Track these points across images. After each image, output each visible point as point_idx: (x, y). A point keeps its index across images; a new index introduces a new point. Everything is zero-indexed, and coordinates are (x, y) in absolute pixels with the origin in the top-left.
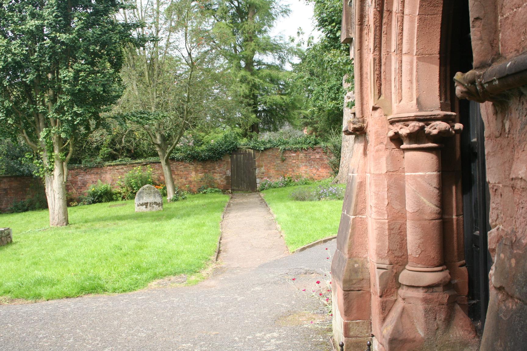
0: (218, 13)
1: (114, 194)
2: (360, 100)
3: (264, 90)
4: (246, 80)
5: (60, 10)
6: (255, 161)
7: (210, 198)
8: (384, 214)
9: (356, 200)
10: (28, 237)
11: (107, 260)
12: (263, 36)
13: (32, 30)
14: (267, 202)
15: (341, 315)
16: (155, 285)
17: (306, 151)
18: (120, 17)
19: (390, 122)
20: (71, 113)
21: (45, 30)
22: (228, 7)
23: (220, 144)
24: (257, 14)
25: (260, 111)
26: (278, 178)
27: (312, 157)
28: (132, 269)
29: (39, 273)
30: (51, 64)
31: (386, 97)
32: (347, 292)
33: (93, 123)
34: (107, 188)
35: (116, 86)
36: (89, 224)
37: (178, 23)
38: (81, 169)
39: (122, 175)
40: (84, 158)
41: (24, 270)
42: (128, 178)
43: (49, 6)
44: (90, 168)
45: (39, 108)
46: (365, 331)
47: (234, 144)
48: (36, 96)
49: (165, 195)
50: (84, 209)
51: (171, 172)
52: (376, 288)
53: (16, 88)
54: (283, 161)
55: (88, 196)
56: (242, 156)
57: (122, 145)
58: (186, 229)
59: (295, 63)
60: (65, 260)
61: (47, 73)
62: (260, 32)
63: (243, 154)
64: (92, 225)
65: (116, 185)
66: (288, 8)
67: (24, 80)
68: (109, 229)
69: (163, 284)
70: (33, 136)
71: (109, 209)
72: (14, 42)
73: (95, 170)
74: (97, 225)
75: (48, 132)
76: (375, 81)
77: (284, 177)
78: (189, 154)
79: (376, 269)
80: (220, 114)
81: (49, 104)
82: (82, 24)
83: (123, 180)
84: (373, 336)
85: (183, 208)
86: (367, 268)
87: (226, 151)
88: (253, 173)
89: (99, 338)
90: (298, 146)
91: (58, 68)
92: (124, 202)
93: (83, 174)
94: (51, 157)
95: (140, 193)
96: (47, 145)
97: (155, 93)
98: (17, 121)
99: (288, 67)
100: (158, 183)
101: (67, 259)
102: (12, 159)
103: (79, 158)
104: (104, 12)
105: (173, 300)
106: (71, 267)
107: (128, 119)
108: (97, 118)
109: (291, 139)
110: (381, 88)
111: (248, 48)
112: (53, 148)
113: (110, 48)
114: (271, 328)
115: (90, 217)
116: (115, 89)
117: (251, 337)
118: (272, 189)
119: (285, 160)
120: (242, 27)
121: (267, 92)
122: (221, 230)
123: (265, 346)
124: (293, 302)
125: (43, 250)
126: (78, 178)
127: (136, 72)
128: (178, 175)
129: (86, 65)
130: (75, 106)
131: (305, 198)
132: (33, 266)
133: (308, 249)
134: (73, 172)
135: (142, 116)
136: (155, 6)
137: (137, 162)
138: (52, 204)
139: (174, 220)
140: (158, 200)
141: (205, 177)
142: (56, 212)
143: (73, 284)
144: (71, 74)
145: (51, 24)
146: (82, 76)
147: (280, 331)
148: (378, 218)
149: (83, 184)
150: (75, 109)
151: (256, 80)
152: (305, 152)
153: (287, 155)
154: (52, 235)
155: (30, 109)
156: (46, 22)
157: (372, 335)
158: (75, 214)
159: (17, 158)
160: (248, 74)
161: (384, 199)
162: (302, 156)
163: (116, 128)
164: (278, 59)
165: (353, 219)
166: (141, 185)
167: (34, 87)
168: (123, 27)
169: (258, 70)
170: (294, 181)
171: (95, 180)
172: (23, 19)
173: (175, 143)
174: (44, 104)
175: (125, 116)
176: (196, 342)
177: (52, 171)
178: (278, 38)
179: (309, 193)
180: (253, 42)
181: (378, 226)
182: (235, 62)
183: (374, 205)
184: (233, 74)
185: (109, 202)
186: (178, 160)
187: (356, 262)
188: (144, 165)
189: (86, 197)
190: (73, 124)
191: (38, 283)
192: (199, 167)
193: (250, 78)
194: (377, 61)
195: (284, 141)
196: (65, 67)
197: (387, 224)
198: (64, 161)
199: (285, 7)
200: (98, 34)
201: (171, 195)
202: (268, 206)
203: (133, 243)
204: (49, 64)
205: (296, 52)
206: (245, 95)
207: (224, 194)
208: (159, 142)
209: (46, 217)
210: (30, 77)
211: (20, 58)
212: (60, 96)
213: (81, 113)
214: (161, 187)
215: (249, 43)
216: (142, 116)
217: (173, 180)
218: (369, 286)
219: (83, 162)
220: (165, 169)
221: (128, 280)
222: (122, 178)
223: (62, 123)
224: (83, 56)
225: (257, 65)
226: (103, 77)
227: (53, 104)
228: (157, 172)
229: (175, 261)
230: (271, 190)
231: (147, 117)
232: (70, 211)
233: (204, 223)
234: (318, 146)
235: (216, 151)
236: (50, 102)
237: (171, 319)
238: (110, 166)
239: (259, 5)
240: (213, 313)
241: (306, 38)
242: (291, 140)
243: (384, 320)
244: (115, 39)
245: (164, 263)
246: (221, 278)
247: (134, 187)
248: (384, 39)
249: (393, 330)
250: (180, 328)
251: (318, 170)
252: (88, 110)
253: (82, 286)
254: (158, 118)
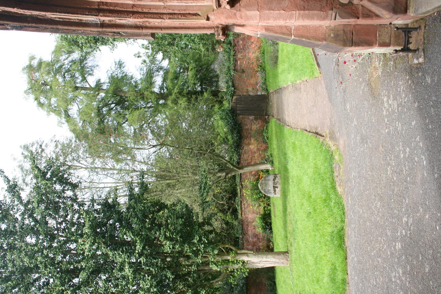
0: (121, 120)
1: (265, 212)
2: (201, 30)
3: (184, 85)
4: (175, 99)
5: (117, 249)
6: (243, 95)
7: (272, 134)
8: (292, 14)
9: (280, 34)
10: (297, 284)
11: (318, 225)
12: (139, 84)
13: (133, 271)
14: (278, 88)
15: (372, 48)
16: (340, 188)
17: (236, 52)
18: (123, 200)
19: (219, 7)
20: (199, 245)
21: (132, 261)
22: (115, 113)
23: (227, 124)
24: (122, 89)
25: (201, 89)
26: (258, 77)
28: (326, 206)
29: (325, 279)
30: (160, 258)
31: (199, 10)
32: (353, 44)
33: (207, 228)
34: (260, 218)
35: (178, 208)
36: (289, 235)
37: (129, 154)
38: (243, 237)
39: (249, 205)
40: (235, 235)
41: (323, 290)
42: (252, 200)
43: (114, 257)
44: (242, 230)
45: (193, 269)
46: (386, 30)
47: (228, 112)
48: (184, 271)
49: (267, 171)
50: (276, 238)
51: (249, 165)
52: (352, 21)
53: (177, 286)
54: (243, 71)
55: (266, 233)
56: (238, 106)
57: (225, 203)
58: (297, 158)
59: (162, 57)
60: (316, 258)
61: (167, 261)
62: (136, 86)
63: (236, 105)
64: (289, 233)
65: (258, 210)
66: (117, 63)
67: (171, 279)
68: (294, 220)
69: (340, 183)
70: (216, 275)
71: (277, 217)
72: (141, 285)
73: (245, 227)
74: (290, 229)
75: (213, 264)
76: (186, 18)
77: (257, 71)
78: (235, 150)
79: (336, 21)
80: (203, 123)
81: (191, 261)
82: (129, 232)
83: (254, 205)
84: (391, 24)
85: (279, 157)
86: (335, 27)
87: (234, 119)
88: (253, 97)
89: (379, 238)
90: (232, 59)
91: (163, 253)
92: (271, 205)
93: (247, 236)
94: (233, 262)
95: (265, 192)
96: (223, 265)
97: (184, 176)
98: (203, 287)
99: (165, 64)
100: (258, 177)
101: (315, 256)
102: (233, 291)
103: (234, 239)
104: (119, 214)
105: (353, 176)
106: (322, 254)
107: (205, 200)
108: (203, 224)
109: (226, 64)
110: (192, 14)
111: (149, 97)
112: (226, 260)
113: (148, 211)
114: (380, 101)
115: (283, 233)
116: (181, 209)
117: (386, 119)
118: (267, 82)
119: (243, 70)
120: (132, 102)
121: (186, 82)
122: (299, 130)
123: (394, 109)
124: (361, 80)
125: (307, 274)
126: (251, 241)
127: (167, 190)
128: (251, 159)
129: (161, 230)
130: (193, 241)
131: (275, 56)
132: (319, 283)
133: (318, 60)
134: (245, 244)
135: (203, 188)
136: (115, 172)
137: (239, 193)
138: (271, 264)
139: (289, 167)
140: (271, 177)
141: (254, 137)
142: (278, 261)
143: (336, 253)
144: (168, 243)
145: (128, 256)
146: (169, 235)
147: (382, 95)
148: (294, 18)
149: (256, 236)
150: (196, 241)
151: (175, 91)
152: (237, 53)
153: (239, 68)
154: (296, 265)
155: (194, 276)
156: (126, 260)
157: (390, 24)
158: (280, 245)
159: (232, 288)
160: (171, 98)
161: (280, 14)
162: (240, 55)
163: (212, 209)
164: (159, 72)
165: (294, 36)
166: (258, 190)
167: (177, 272)
168: (131, 200)
169: (167, 90)
170: (261, 63)
171: (253, 227)
172: (124, 277)
173: (225, 161)
174: (191, 265)
175: (203, 202)
176: (387, 163)
177: (244, 262)
178: (142, 72)
179: (272, 52)
180: (145, 93)
181: (301, 18)
182: (160, 108)
183: (284, 21)
184: (170, 110)
185: (271, 217)
186: (240, 159)
187: (329, 35)
188: (242, 187)
189: (266, 235)
190: (207, 243)
191: (333, 280)
192: (246, 141)
193: (173, 96)
194: (171, 16)
195: (227, 70)
196: (162, 248)
197: (300, 11)
198: (237, 252)
199: (117, 65)
200: (137, 220)
201: (268, 166)
202: (281, 87)
203: (306, 203)
204: (159, 259)
205: (153, 57)
206: (187, 101)
207: (269, 122)
208: (224, 174)
209: (281, 269)
210: (169, 275)
211: (154, 281)
212: (185, 253)
213: (199, 237)
214: (261, 173)
215: (145, 96)
216: (203, 188)
217: (256, 164)
218: (349, 26)
219: (237, 236)
220: (246, 170)
221: (335, 210)
222: (252, 205)
223: (206, 252)
224: (154, 233)
225: (163, 90)
226: (171, 218)
227: (191, 258)
228: (249, 176)
229: (322, 171)
230: (267, 83)
231: (204, 184)
232: (277, 248)
233: (292, 143)
234: (232, 42)
235: (233, 127)
236: (190, 260)
237: (368, 180)
238: (242, 214)
239: (114, 87)
240: (365, 146)
241: (143, 51)
242: (227, 64)
243: (377, 16)
244: (141, 207)
245: (323, 180)
246: (338, 135)
247: (260, 196)
248: (154, 11)
249: (386, 10)
250: (375, 174)
251: (252, 43)
252: (197, 231)
253: (338, 247)
254: (205, 176)
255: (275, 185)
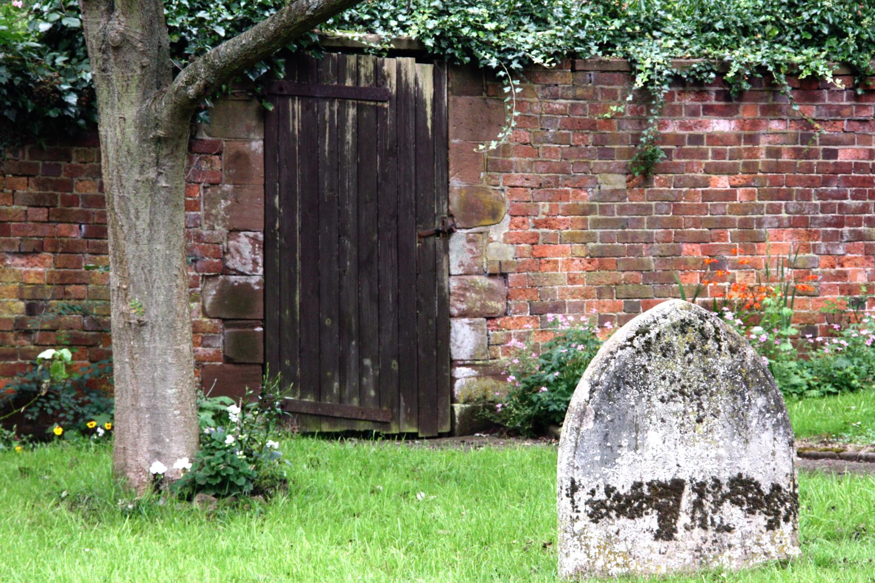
27: (845, 155)
63: (358, 95)
255: (687, 499)
